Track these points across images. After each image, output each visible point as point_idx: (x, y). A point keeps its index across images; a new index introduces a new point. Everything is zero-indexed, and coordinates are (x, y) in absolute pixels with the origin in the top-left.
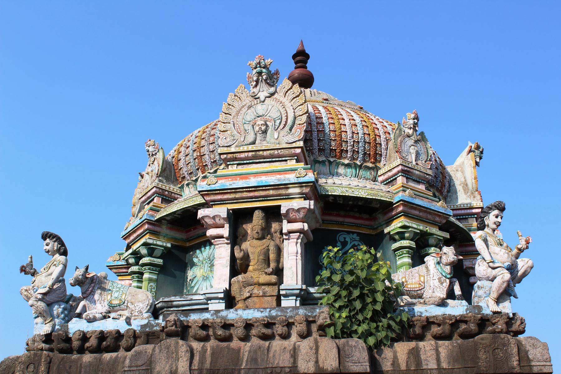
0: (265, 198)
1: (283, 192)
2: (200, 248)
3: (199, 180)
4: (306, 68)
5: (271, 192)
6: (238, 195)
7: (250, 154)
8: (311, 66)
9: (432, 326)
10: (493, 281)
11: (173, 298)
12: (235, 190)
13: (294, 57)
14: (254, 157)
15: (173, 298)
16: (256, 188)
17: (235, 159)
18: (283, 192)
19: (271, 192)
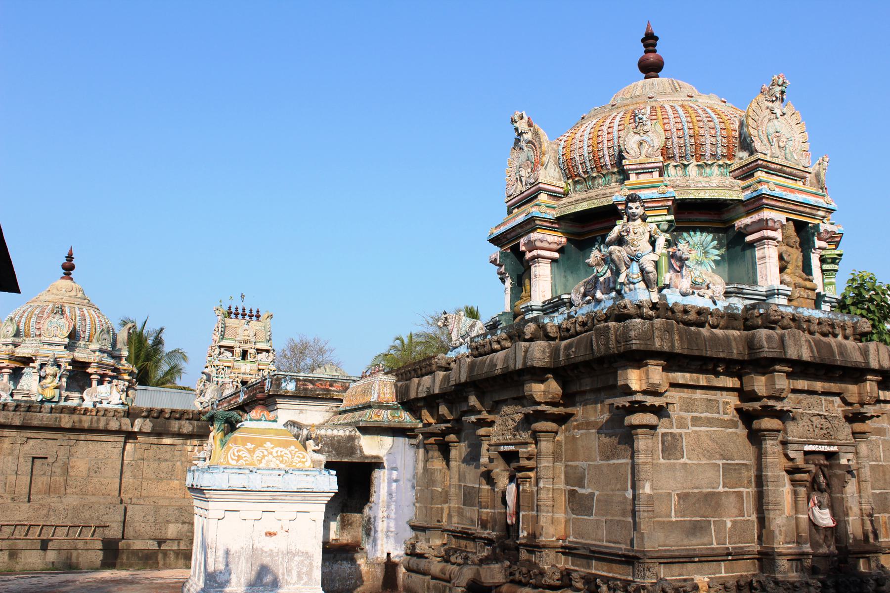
0: (800, 213)
1: (814, 212)
2: (695, 231)
3: (691, 166)
4: (655, 51)
5: (807, 210)
6: (786, 206)
7: (779, 167)
8: (661, 49)
9: (279, 400)
10: (232, 347)
11: (743, 286)
12: (787, 201)
13: (643, 41)
14: (780, 171)
15: (743, 286)
16: (801, 204)
17: (766, 167)
18: (814, 212)
19: (807, 210)
